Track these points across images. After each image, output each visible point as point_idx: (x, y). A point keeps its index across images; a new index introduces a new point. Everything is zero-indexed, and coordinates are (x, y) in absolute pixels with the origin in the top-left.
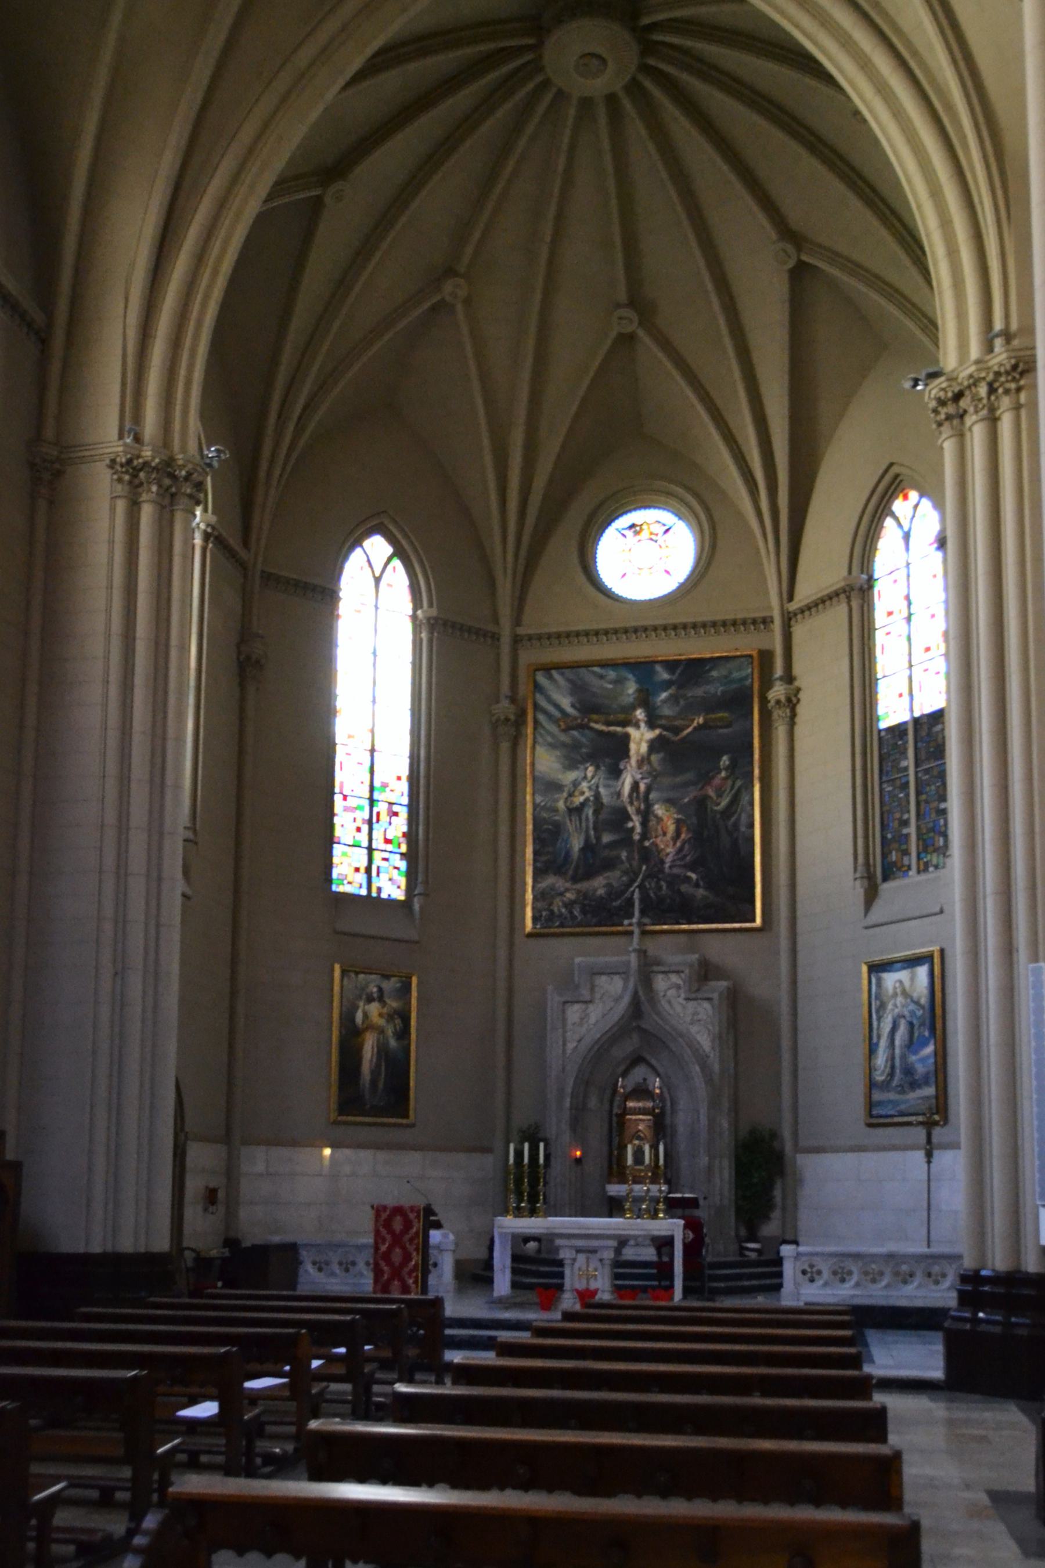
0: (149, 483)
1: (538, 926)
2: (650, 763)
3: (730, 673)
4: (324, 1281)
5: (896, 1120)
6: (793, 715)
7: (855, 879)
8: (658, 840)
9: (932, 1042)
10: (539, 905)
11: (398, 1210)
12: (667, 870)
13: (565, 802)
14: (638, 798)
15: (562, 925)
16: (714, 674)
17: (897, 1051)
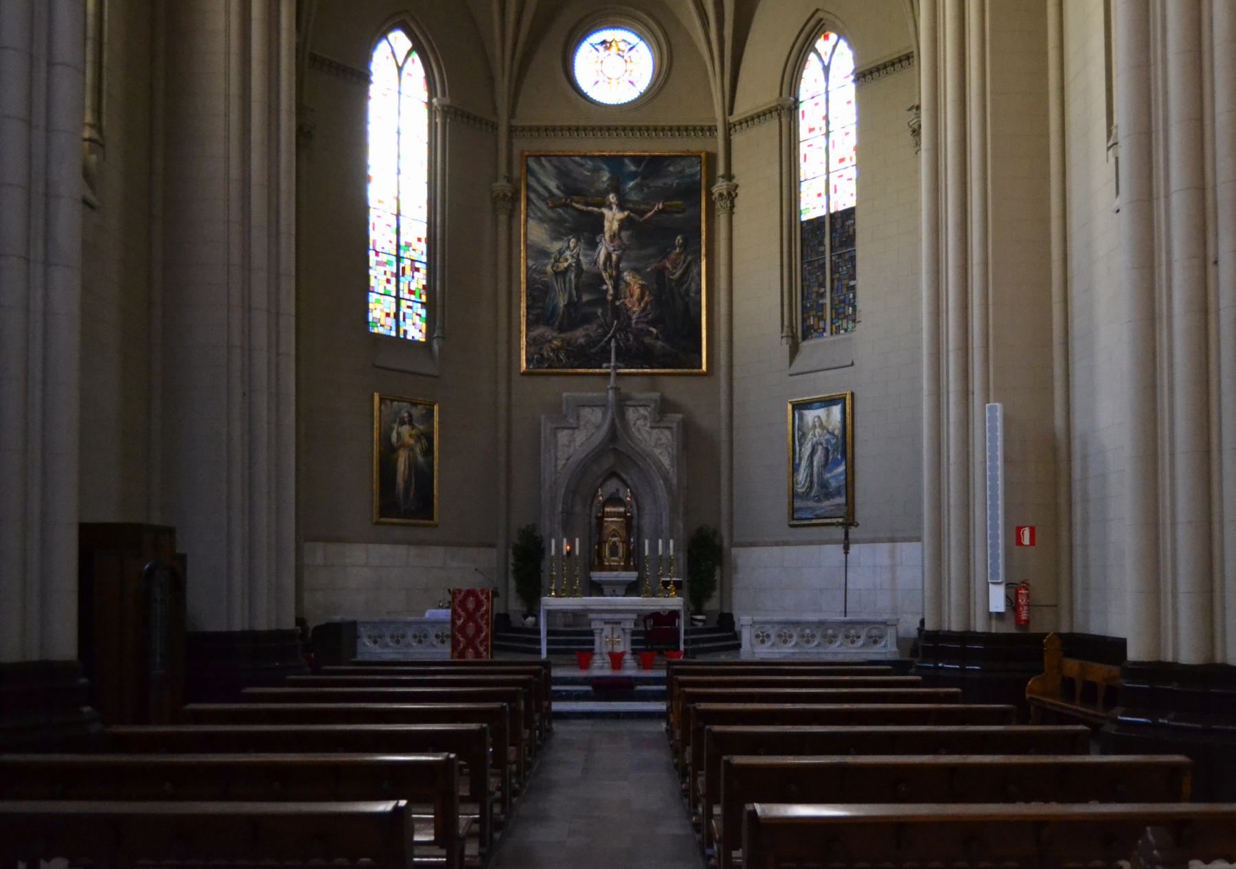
1: (531, 367)
2: (620, 238)
3: (683, 170)
4: (379, 651)
5: (814, 521)
6: (732, 206)
7: (782, 337)
8: (627, 301)
9: (844, 463)
10: (532, 350)
11: (471, 593)
12: (633, 325)
13: (552, 267)
14: (611, 265)
15: (550, 367)
16: (671, 169)
17: (815, 470)
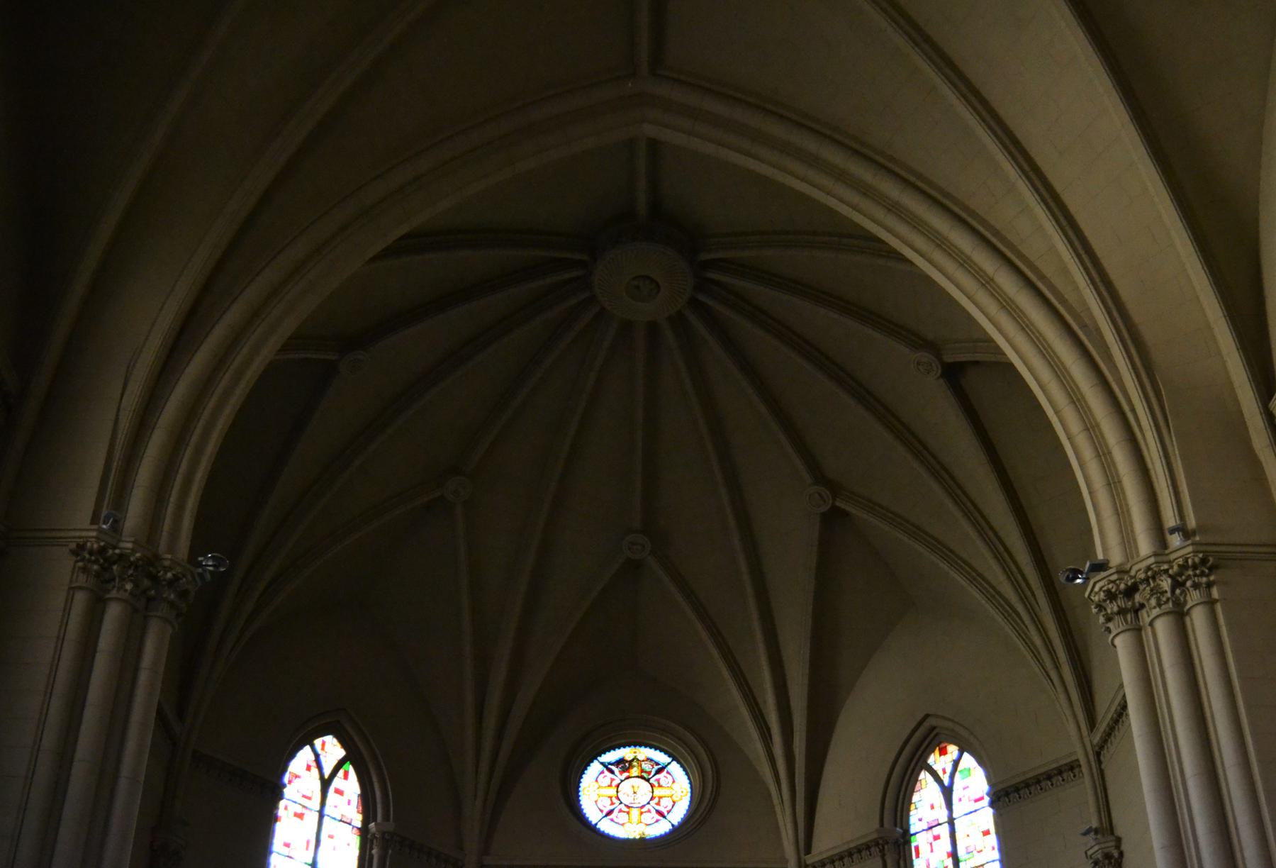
0: (122, 579)
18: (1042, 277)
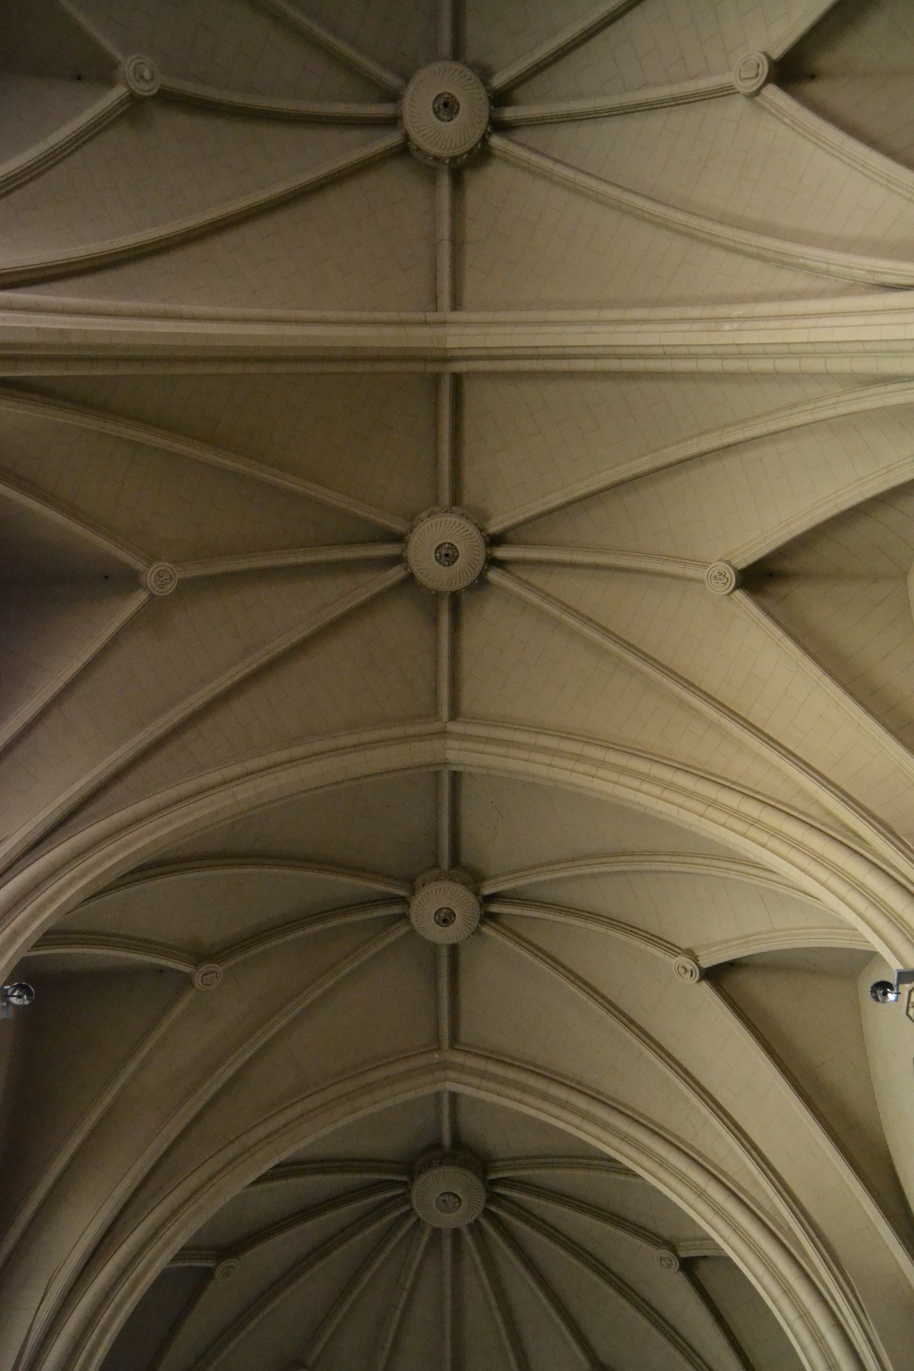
18: (741, 1189)
